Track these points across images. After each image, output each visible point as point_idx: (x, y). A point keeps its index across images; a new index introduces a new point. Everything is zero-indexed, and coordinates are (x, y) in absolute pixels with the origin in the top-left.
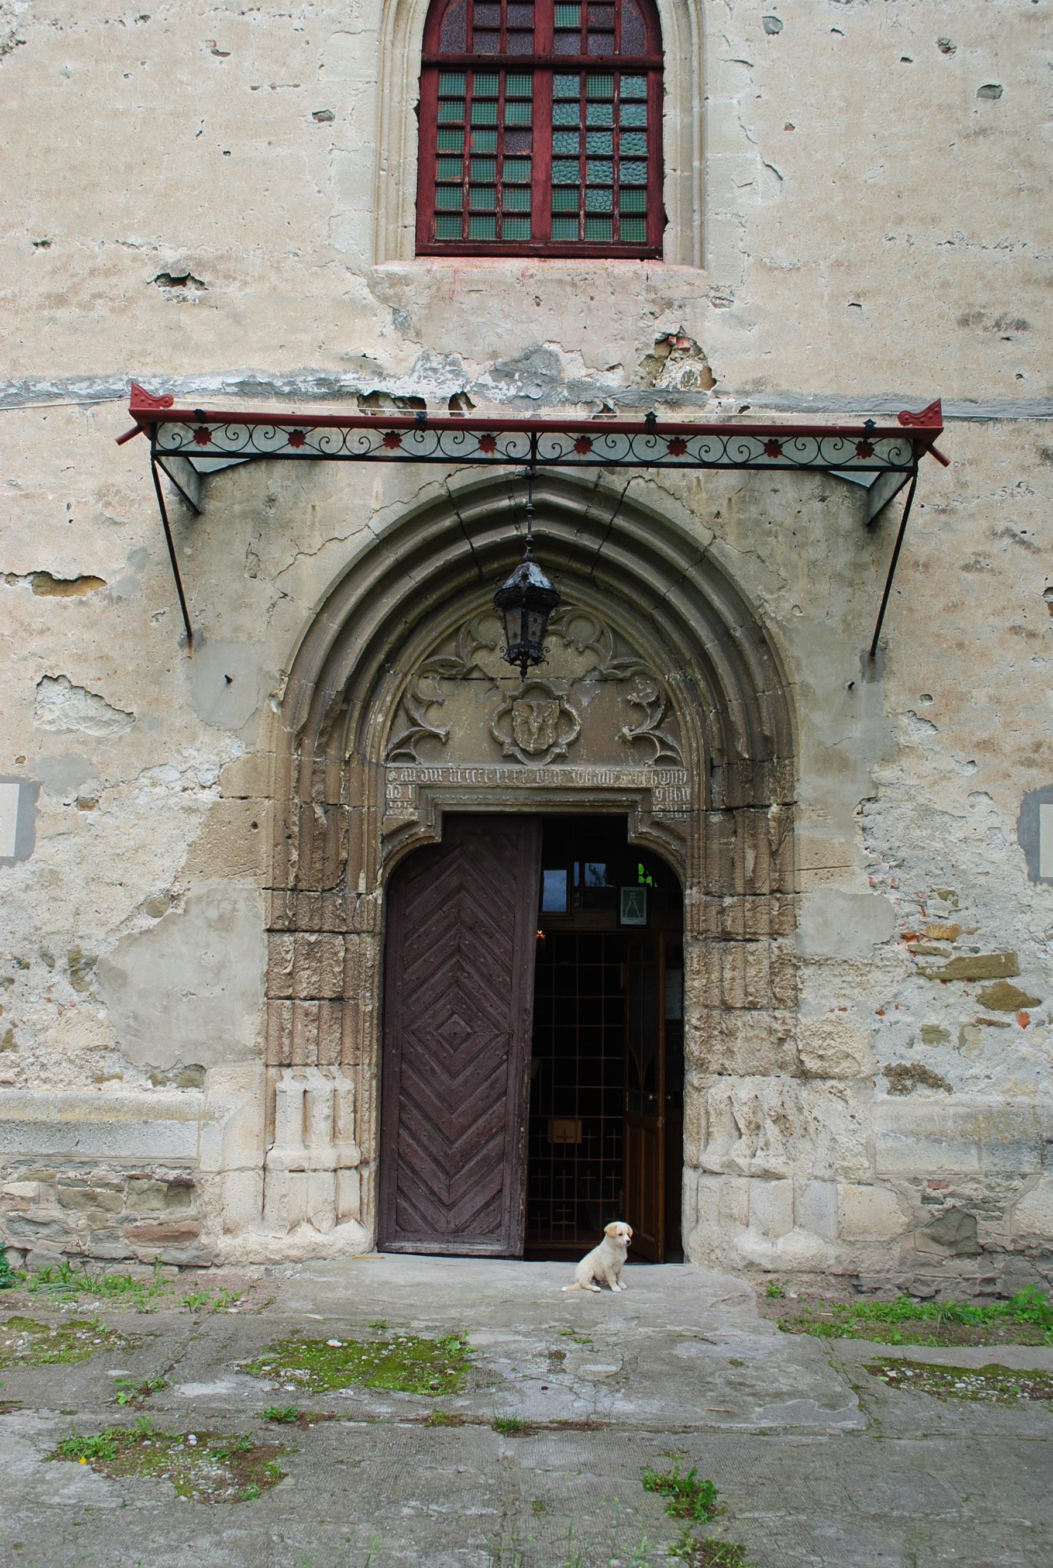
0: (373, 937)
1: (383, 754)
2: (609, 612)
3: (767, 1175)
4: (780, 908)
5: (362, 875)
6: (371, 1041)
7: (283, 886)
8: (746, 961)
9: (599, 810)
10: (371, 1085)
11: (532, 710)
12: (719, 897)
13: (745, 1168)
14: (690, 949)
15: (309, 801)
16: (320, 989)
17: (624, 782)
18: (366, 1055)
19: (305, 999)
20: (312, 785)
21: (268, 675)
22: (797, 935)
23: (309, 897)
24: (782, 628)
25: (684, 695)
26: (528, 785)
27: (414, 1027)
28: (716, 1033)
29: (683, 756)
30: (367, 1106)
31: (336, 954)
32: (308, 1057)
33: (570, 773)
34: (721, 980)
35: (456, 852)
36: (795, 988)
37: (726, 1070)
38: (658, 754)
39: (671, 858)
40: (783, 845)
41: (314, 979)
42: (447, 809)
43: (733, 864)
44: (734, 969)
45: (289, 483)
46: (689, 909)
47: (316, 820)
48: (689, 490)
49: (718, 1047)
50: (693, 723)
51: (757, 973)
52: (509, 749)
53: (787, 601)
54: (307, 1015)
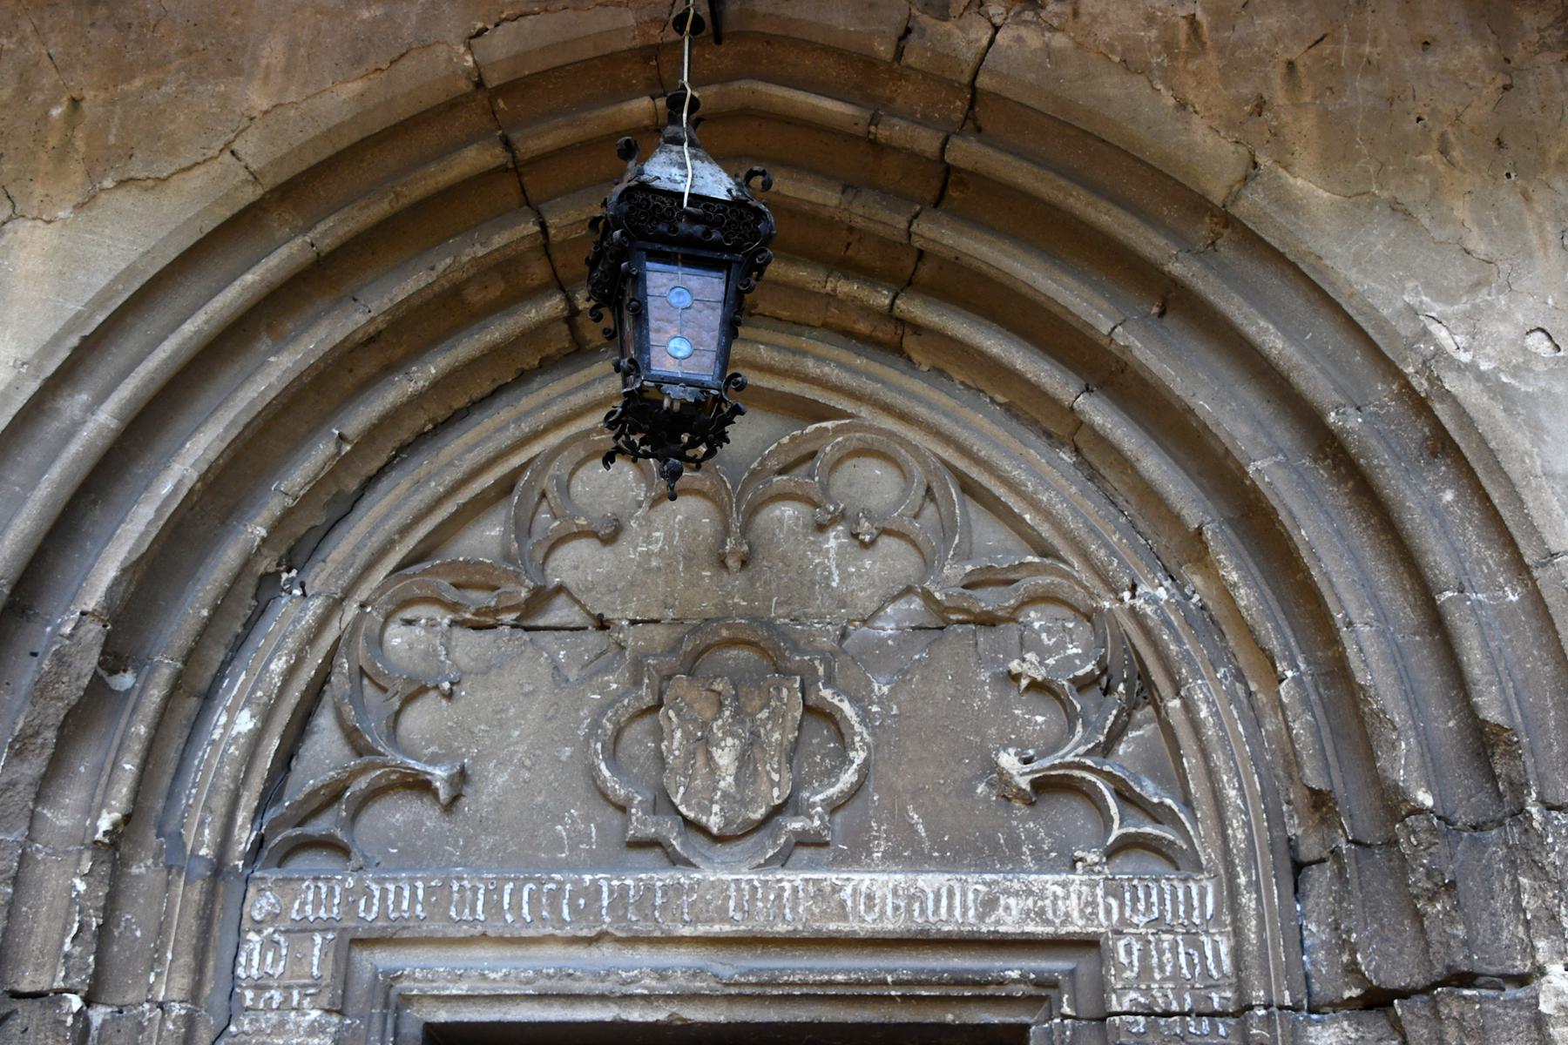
1: (244, 837)
9: (932, 1016)
11: (721, 705)
17: (1010, 919)
26: (702, 930)
33: (836, 889)
38: (1116, 831)
42: (442, 1016)
48: (1169, 46)
50: (1220, 725)
52: (641, 824)
53: (1505, 317)
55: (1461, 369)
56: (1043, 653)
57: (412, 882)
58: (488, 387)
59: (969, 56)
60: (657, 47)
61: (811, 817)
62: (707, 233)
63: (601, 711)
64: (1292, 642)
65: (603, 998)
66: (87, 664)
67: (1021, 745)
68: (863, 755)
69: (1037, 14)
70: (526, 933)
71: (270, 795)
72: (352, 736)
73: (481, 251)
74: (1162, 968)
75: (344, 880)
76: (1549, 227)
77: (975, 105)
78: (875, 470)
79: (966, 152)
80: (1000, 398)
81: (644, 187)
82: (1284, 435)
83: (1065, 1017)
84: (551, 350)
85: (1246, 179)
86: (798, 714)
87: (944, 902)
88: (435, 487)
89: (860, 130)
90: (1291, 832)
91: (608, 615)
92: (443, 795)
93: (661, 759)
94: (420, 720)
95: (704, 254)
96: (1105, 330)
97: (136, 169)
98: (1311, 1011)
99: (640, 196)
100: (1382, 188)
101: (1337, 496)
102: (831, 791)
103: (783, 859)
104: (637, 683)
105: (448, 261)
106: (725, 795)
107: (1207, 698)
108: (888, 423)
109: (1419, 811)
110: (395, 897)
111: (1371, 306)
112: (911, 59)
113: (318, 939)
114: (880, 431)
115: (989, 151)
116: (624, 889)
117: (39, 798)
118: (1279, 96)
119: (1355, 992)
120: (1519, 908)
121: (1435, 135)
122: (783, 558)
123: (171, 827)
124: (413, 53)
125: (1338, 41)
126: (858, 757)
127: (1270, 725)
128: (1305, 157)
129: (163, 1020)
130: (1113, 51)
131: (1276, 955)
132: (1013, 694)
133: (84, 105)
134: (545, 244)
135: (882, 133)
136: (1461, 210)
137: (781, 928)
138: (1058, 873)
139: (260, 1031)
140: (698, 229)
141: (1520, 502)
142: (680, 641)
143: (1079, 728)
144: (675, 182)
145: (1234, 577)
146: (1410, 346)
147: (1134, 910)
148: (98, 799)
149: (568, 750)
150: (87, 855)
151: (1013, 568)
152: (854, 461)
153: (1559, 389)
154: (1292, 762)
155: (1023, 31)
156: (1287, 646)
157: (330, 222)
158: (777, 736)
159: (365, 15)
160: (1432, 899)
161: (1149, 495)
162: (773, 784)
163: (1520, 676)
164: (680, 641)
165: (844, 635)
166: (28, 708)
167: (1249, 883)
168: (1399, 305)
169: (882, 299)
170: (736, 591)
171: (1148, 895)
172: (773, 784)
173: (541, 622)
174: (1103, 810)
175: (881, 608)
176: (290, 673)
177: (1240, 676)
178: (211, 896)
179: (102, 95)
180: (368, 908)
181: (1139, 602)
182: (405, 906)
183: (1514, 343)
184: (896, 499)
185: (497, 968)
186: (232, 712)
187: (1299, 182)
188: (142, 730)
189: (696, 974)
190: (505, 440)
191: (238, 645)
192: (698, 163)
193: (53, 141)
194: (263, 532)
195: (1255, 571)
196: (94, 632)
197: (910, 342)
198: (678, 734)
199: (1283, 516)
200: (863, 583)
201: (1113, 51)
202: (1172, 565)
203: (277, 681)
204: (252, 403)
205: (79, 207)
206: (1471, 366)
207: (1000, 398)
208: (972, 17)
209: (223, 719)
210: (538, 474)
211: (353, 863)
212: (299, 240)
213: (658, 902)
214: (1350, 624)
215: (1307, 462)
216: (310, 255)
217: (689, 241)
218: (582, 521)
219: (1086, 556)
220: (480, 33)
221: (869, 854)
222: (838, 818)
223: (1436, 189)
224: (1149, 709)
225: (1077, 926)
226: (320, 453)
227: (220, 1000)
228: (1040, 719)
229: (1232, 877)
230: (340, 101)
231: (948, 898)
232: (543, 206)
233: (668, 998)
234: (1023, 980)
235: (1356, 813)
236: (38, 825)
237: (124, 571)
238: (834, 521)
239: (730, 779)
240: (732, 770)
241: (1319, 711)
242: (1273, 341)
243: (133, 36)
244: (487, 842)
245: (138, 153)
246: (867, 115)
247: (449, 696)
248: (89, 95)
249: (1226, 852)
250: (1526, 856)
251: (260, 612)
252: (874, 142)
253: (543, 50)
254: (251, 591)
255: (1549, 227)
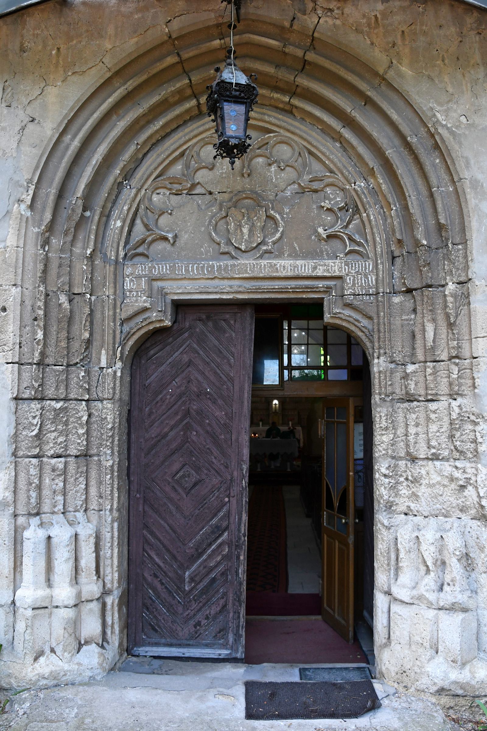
0: (113, 403)
1: (122, 254)
2: (305, 135)
3: (452, 608)
4: (459, 371)
5: (103, 352)
6: (112, 491)
7: (30, 361)
8: (428, 419)
10: (112, 528)
11: (244, 216)
12: (403, 365)
13: (434, 602)
14: (378, 409)
15: (55, 290)
16: (66, 448)
17: (320, 272)
18: (107, 502)
19: (52, 457)
20: (59, 277)
21: (18, 184)
22: (475, 395)
23: (55, 371)
24: (452, 133)
25: (367, 199)
26: (241, 276)
27: (153, 476)
28: (402, 479)
29: (370, 249)
30: (109, 545)
31: (80, 418)
32: (55, 506)
33: (275, 265)
34: (406, 435)
35: (186, 335)
36: (475, 441)
37: (411, 510)
38: (348, 249)
39: (360, 334)
40: (459, 318)
41: (61, 439)
42: (176, 297)
43: (414, 336)
44: (417, 425)
45: (39, 32)
46: (377, 375)
47: (60, 305)
48: (369, 25)
49: (404, 491)
50: (376, 221)
51: (438, 430)
53: (455, 111)
54: (54, 470)
55: (443, 126)
56: (330, 200)
57: (165, 264)
58: (175, 126)
59: (312, 27)
60: (221, 23)
61: (268, 246)
62: (240, 94)
63: (212, 217)
64: (396, 199)
65: (216, 293)
66: (79, 211)
67: (324, 226)
68: (282, 229)
69: (332, 14)
70: (196, 277)
71: (127, 243)
72: (146, 226)
73: (173, 89)
74: (358, 283)
75: (148, 264)
76: (469, 85)
77: (314, 42)
78: (285, 147)
79: (311, 56)
80: (320, 127)
81: (223, 81)
82: (397, 141)
83: (333, 296)
84: (193, 114)
85: (389, 67)
86: (264, 218)
87: (303, 268)
88: (163, 156)
89: (280, 49)
90: (392, 248)
91: (212, 191)
92: (171, 241)
93: (228, 231)
94: (163, 221)
95: (239, 100)
96: (349, 111)
97: (77, 69)
98: (394, 293)
99: (221, 84)
100: (426, 71)
101: (409, 159)
102: (274, 239)
103: (261, 257)
104: (221, 210)
105: (164, 92)
106: (246, 240)
107: (373, 213)
108: (289, 135)
109: (423, 245)
110: (162, 269)
111: (421, 107)
112: (295, 27)
113: (143, 279)
114: (286, 137)
115: (317, 56)
116: (220, 266)
117: (72, 246)
118: (399, 42)
119: (404, 289)
120: (444, 269)
121: (441, 56)
122: (259, 173)
123: (103, 251)
124: (151, 29)
125: (416, 25)
126: (281, 229)
127: (389, 221)
128: (406, 61)
129: (108, 300)
130: (353, 26)
131: (386, 280)
132: (322, 211)
133: (61, 50)
134: (191, 85)
135: (287, 50)
136: (446, 79)
137: (261, 275)
138: (333, 260)
139: (132, 302)
140: (238, 93)
141: (454, 164)
142: (232, 198)
143: (339, 221)
144: (231, 79)
145: (381, 181)
146: (430, 119)
147: (352, 269)
148: (86, 245)
149: (203, 228)
150: (85, 260)
151: (322, 176)
152: (279, 145)
153: (467, 133)
154: (394, 231)
155: (328, 19)
156: (394, 200)
157: (131, 82)
158: (259, 224)
159: (136, 17)
160: (424, 267)
161: (359, 156)
162: (258, 237)
163: (450, 210)
164: (232, 198)
165: (277, 195)
166: (67, 223)
167: (381, 262)
168: (428, 107)
169: (287, 99)
170: (246, 183)
171: (355, 265)
172: (258, 237)
173: (194, 193)
174: (345, 243)
175: (287, 187)
176: (129, 209)
177: (382, 207)
178: (116, 269)
179: (65, 46)
180: (155, 271)
181: (356, 187)
182: (164, 271)
183: (457, 119)
184: (291, 153)
185: (189, 286)
186: (115, 221)
187: (404, 68)
188: (95, 227)
189: (240, 286)
190: (181, 141)
191: (114, 202)
192: (236, 71)
193: (54, 62)
194: (119, 172)
195: (387, 179)
196: (80, 202)
197: (294, 110)
198: (233, 224)
199: (394, 166)
200: (282, 181)
201: (353, 26)
202: (365, 176)
203: (126, 212)
204: (114, 137)
205: (63, 81)
206: (446, 126)
207: (320, 127)
208: (313, 14)
209: (113, 223)
210: (191, 151)
211: (150, 259)
212: (123, 88)
213: (229, 269)
214: (410, 197)
215: (402, 149)
216: (126, 92)
217: (235, 97)
218: (204, 164)
219: (342, 174)
220: (170, 21)
221: (284, 255)
222: (276, 245)
223: (440, 72)
224: (358, 215)
225: (337, 273)
226: (132, 149)
227: (121, 295)
228: (329, 218)
229: (377, 261)
230: (131, 45)
231: (305, 267)
232: (190, 74)
233: (233, 293)
234: (323, 287)
235: (409, 245)
236: (72, 252)
237: (86, 186)
238: (273, 163)
239: (247, 236)
240: (247, 233)
241: (401, 218)
242: (395, 116)
243: (72, 27)
244: (183, 253)
245: (76, 64)
246: (282, 45)
247: (171, 214)
248: (62, 46)
249: (376, 254)
250: (446, 256)
251: (119, 193)
252: (284, 52)
253: (188, 26)
254: (116, 187)
255: (469, 85)
